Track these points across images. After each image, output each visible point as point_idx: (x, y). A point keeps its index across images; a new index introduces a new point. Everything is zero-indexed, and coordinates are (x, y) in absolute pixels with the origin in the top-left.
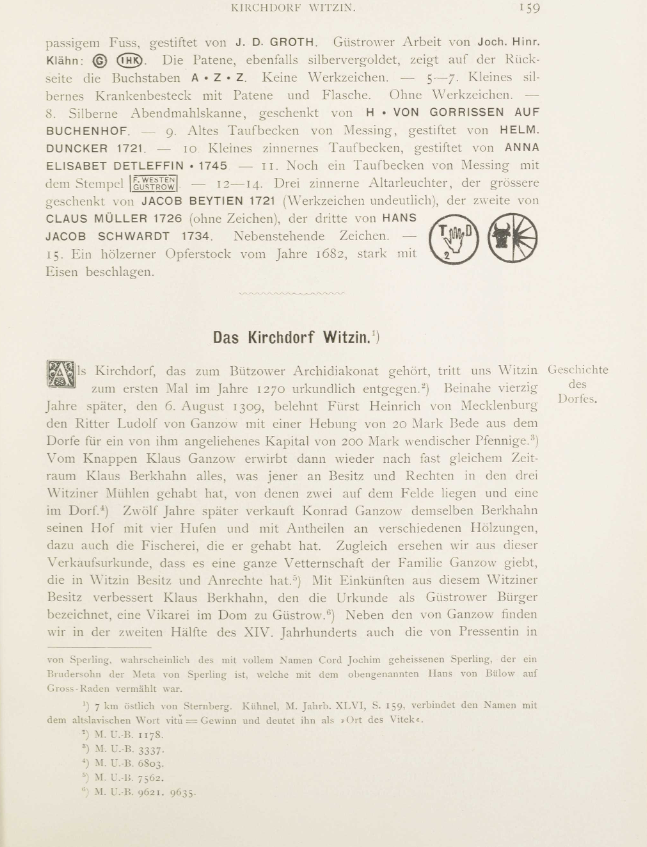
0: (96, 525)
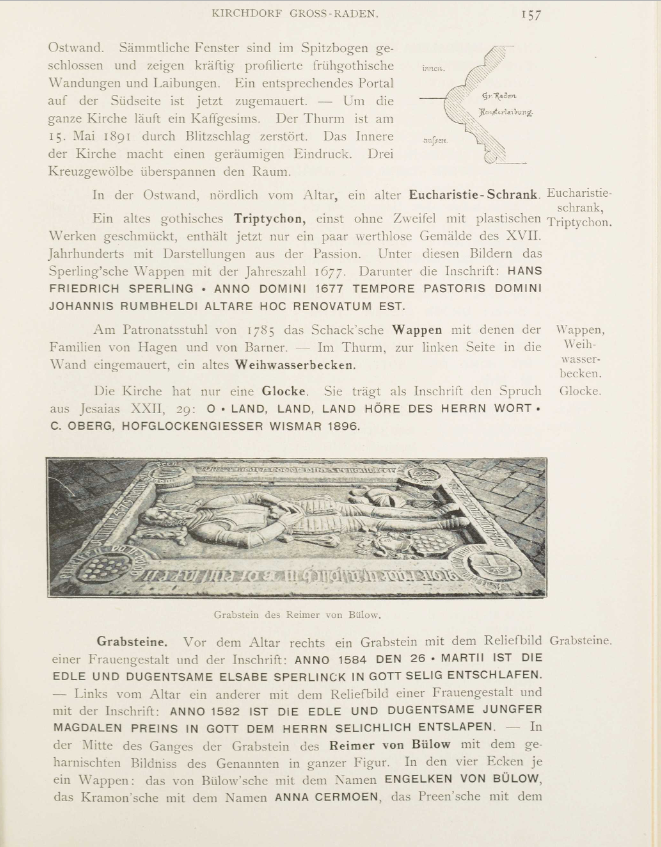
0: (143, 344)
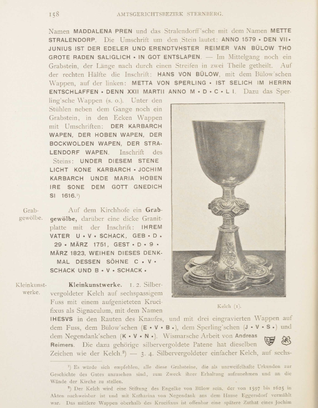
0: (91, 73)
